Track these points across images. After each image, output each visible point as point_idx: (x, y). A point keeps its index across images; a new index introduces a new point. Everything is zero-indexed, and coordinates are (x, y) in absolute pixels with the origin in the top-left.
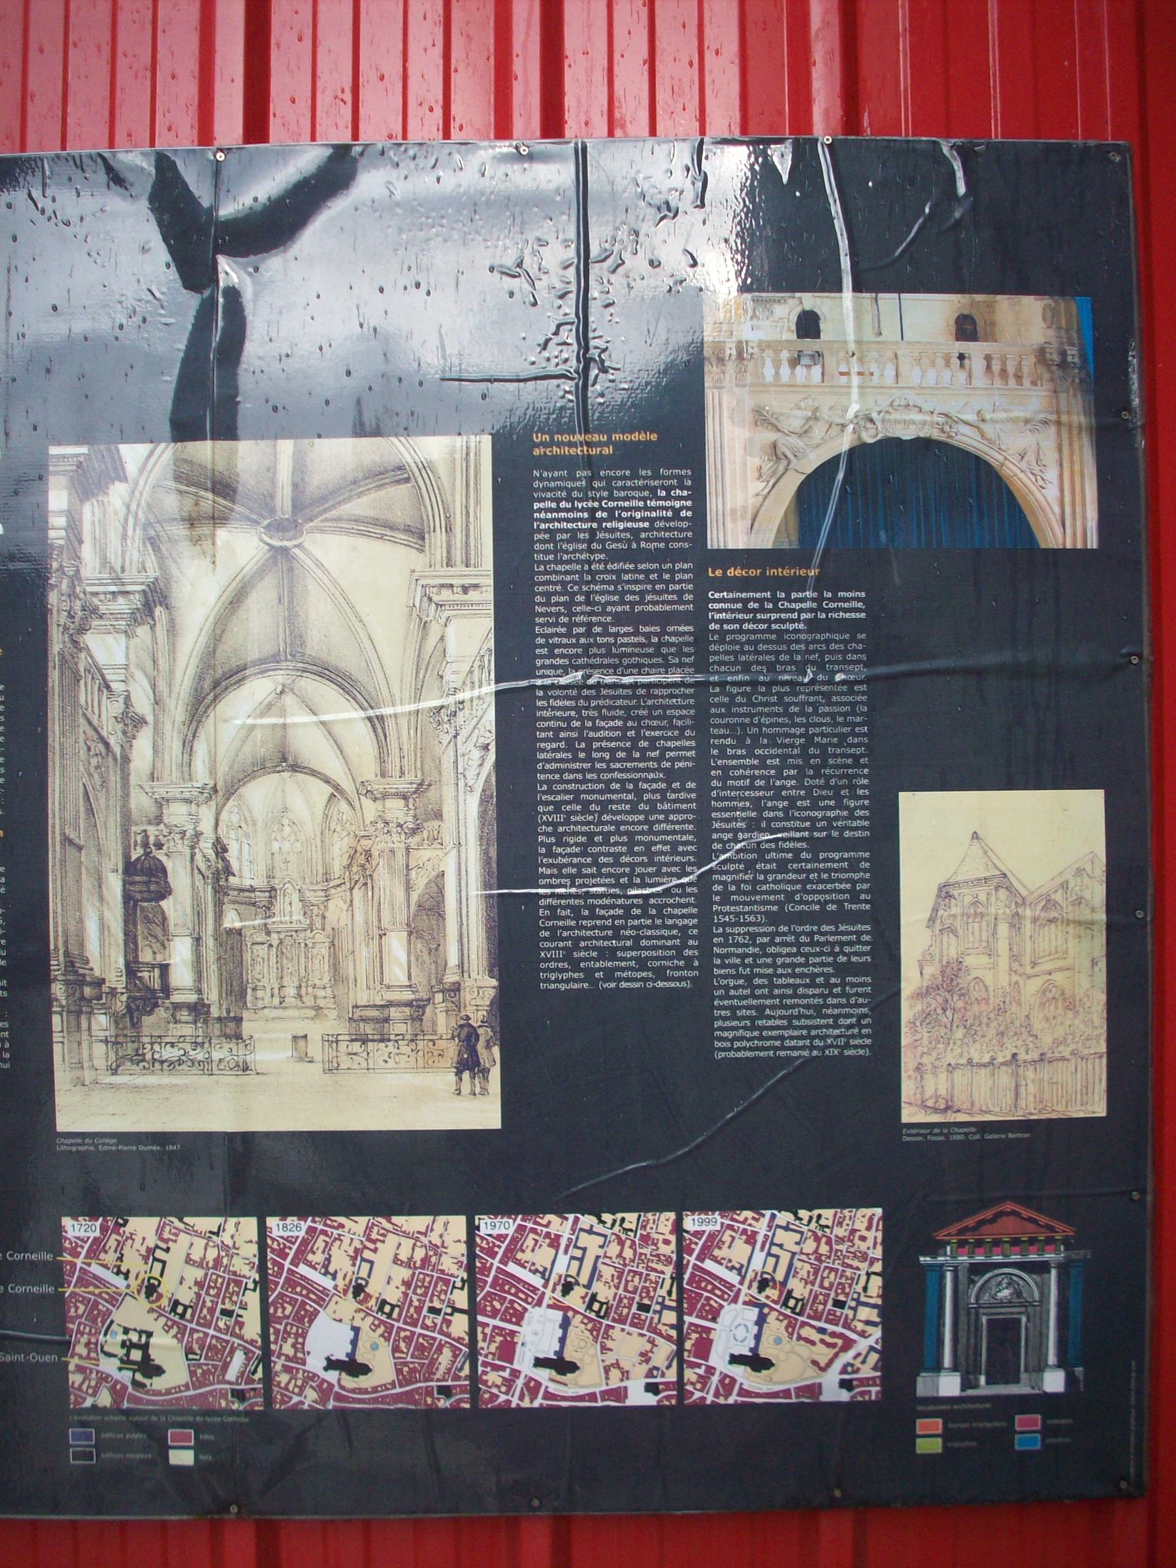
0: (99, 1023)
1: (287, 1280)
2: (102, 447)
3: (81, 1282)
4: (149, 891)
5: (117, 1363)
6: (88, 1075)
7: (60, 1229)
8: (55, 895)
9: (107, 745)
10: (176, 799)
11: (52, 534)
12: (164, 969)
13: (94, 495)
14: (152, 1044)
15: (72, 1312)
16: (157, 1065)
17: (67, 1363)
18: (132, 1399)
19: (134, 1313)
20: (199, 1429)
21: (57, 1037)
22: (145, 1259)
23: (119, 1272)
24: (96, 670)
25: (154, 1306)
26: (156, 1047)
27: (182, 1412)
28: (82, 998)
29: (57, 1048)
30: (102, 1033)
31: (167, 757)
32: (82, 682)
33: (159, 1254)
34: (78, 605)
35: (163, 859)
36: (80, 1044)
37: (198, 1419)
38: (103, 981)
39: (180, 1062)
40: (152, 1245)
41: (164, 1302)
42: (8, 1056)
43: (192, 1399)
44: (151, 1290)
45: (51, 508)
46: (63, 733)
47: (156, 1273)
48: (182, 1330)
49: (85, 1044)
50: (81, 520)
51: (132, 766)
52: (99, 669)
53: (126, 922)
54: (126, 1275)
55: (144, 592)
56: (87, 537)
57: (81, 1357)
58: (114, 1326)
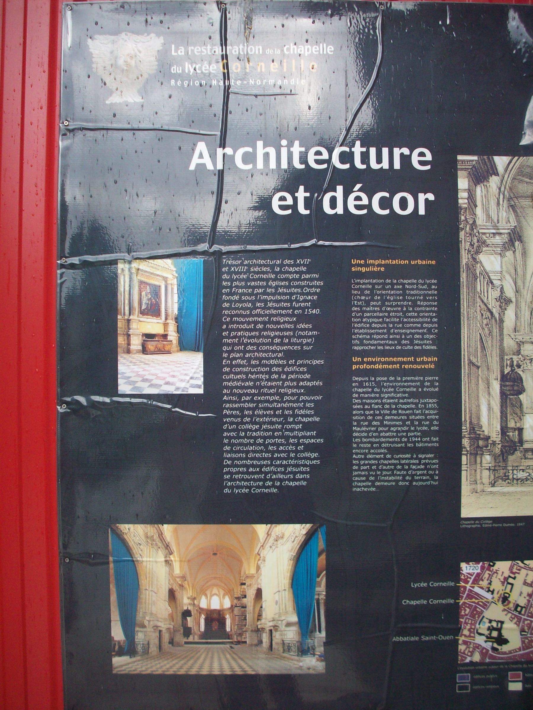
0: (486, 460)
1: (468, 595)
2: (485, 157)
3: (469, 597)
4: (513, 390)
5: (484, 638)
6: (479, 487)
7: (459, 569)
8: (465, 392)
9: (492, 313)
10: (527, 342)
11: (460, 201)
12: (521, 430)
13: (482, 182)
14: (513, 470)
15: (463, 613)
16: (515, 481)
17: (458, 640)
18: (491, 657)
19: (495, 612)
20: (524, 671)
21: (464, 467)
22: (503, 583)
23: (489, 591)
24: (486, 274)
25: (506, 608)
26: (515, 472)
27: (517, 663)
28: (478, 446)
29: (464, 473)
30: (488, 465)
31: (522, 320)
32: (478, 279)
33: (510, 580)
34: (475, 240)
35: (521, 373)
36: (476, 471)
37: (525, 666)
38: (489, 437)
39: (527, 479)
40: (507, 576)
41: (511, 605)
42: (437, 478)
43: (522, 655)
44: (505, 599)
45: (459, 187)
46: (468, 306)
47: (508, 591)
48: (519, 619)
49: (478, 471)
50: (475, 195)
51: (505, 324)
52: (487, 273)
53: (502, 406)
54: (492, 592)
55: (509, 233)
56: (479, 203)
57: (465, 636)
58: (485, 620)
